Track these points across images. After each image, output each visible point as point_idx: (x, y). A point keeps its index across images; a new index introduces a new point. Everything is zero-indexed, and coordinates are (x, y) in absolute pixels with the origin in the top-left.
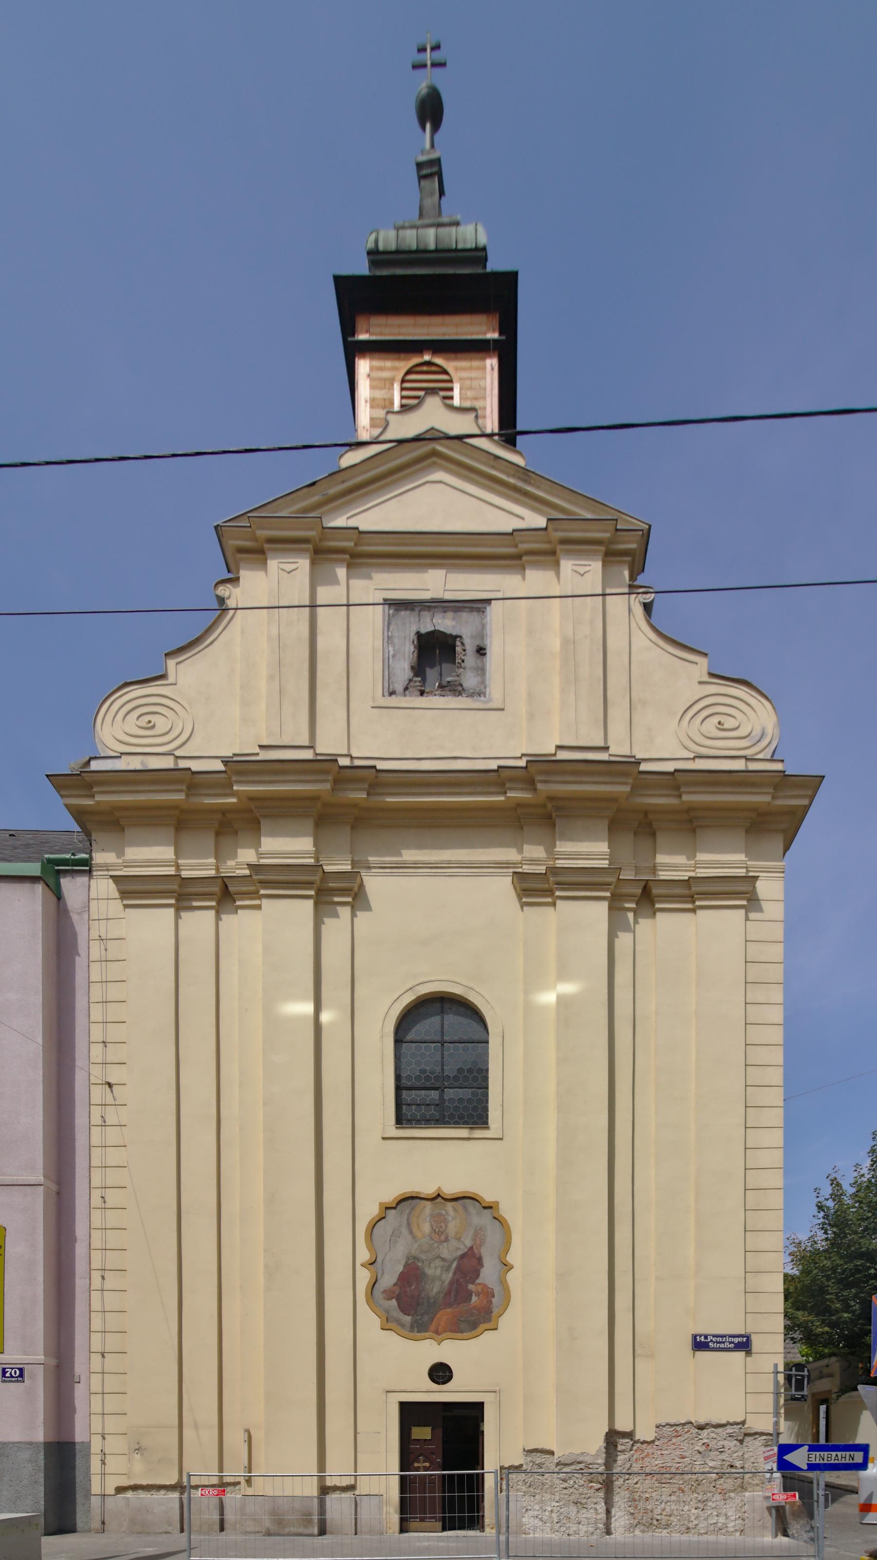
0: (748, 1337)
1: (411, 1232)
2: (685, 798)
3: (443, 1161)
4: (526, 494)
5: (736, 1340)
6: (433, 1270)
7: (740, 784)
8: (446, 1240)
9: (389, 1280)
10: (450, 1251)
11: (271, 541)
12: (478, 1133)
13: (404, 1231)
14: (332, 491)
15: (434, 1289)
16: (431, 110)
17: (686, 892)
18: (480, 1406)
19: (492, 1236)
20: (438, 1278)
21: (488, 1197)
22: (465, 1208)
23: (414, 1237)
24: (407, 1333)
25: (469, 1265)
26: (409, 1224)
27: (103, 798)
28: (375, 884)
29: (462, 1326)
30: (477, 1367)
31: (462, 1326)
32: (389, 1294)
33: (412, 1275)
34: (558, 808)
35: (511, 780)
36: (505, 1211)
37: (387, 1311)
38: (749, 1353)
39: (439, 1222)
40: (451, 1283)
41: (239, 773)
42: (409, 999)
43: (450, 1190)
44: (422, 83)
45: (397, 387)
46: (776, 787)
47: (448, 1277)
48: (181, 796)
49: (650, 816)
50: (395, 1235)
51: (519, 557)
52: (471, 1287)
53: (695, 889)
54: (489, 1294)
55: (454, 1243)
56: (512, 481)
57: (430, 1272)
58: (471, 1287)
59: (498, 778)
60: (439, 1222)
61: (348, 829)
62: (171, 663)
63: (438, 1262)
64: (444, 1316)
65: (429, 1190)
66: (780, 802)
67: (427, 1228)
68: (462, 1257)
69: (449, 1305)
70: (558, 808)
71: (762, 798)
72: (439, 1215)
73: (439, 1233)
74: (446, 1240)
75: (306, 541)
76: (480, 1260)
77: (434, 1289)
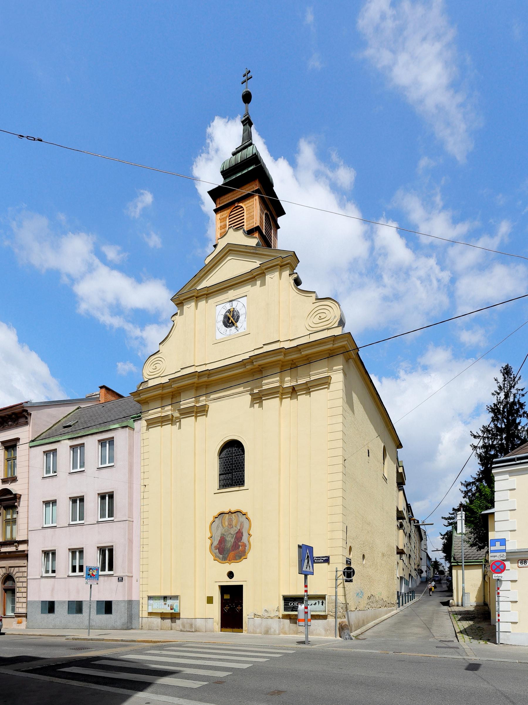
0: (328, 557)
1: (222, 525)
2: (303, 353)
3: (233, 499)
4: (257, 254)
5: (324, 559)
6: (228, 538)
7: (321, 344)
8: (232, 527)
9: (216, 543)
10: (233, 531)
11: (184, 299)
12: (241, 488)
13: (220, 525)
14: (201, 275)
15: (229, 545)
16: (247, 98)
17: (306, 387)
18: (242, 586)
19: (246, 525)
20: (230, 540)
21: (244, 511)
22: (238, 515)
23: (223, 527)
24: (220, 561)
25: (239, 535)
26: (222, 522)
27: (143, 397)
28: (213, 407)
29: (237, 558)
30: (243, 573)
31: (237, 558)
32: (216, 548)
33: (222, 540)
34: (262, 368)
35: (247, 363)
36: (249, 515)
37: (215, 554)
38: (329, 563)
39: (230, 520)
40: (234, 543)
41: (173, 382)
42: (222, 443)
43: (233, 510)
44: (243, 89)
45: (228, 219)
46: (334, 341)
47: (233, 540)
48: (161, 391)
49: (294, 361)
50: (218, 527)
51: (254, 277)
52: (240, 543)
53: (309, 385)
54: (245, 545)
55: (234, 528)
56: (252, 251)
57: (227, 539)
58: (240, 543)
59: (243, 363)
60: (230, 520)
61: (205, 389)
62: (125, 394)
63: (230, 536)
64: (232, 554)
65: (227, 511)
66: (335, 346)
67: (227, 524)
68: (237, 533)
69: (233, 550)
70: (262, 368)
71: (329, 346)
72: (230, 518)
73: (230, 525)
74: (232, 527)
75: (193, 296)
76: (242, 533)
77: (229, 545)
